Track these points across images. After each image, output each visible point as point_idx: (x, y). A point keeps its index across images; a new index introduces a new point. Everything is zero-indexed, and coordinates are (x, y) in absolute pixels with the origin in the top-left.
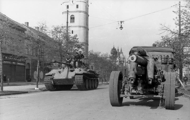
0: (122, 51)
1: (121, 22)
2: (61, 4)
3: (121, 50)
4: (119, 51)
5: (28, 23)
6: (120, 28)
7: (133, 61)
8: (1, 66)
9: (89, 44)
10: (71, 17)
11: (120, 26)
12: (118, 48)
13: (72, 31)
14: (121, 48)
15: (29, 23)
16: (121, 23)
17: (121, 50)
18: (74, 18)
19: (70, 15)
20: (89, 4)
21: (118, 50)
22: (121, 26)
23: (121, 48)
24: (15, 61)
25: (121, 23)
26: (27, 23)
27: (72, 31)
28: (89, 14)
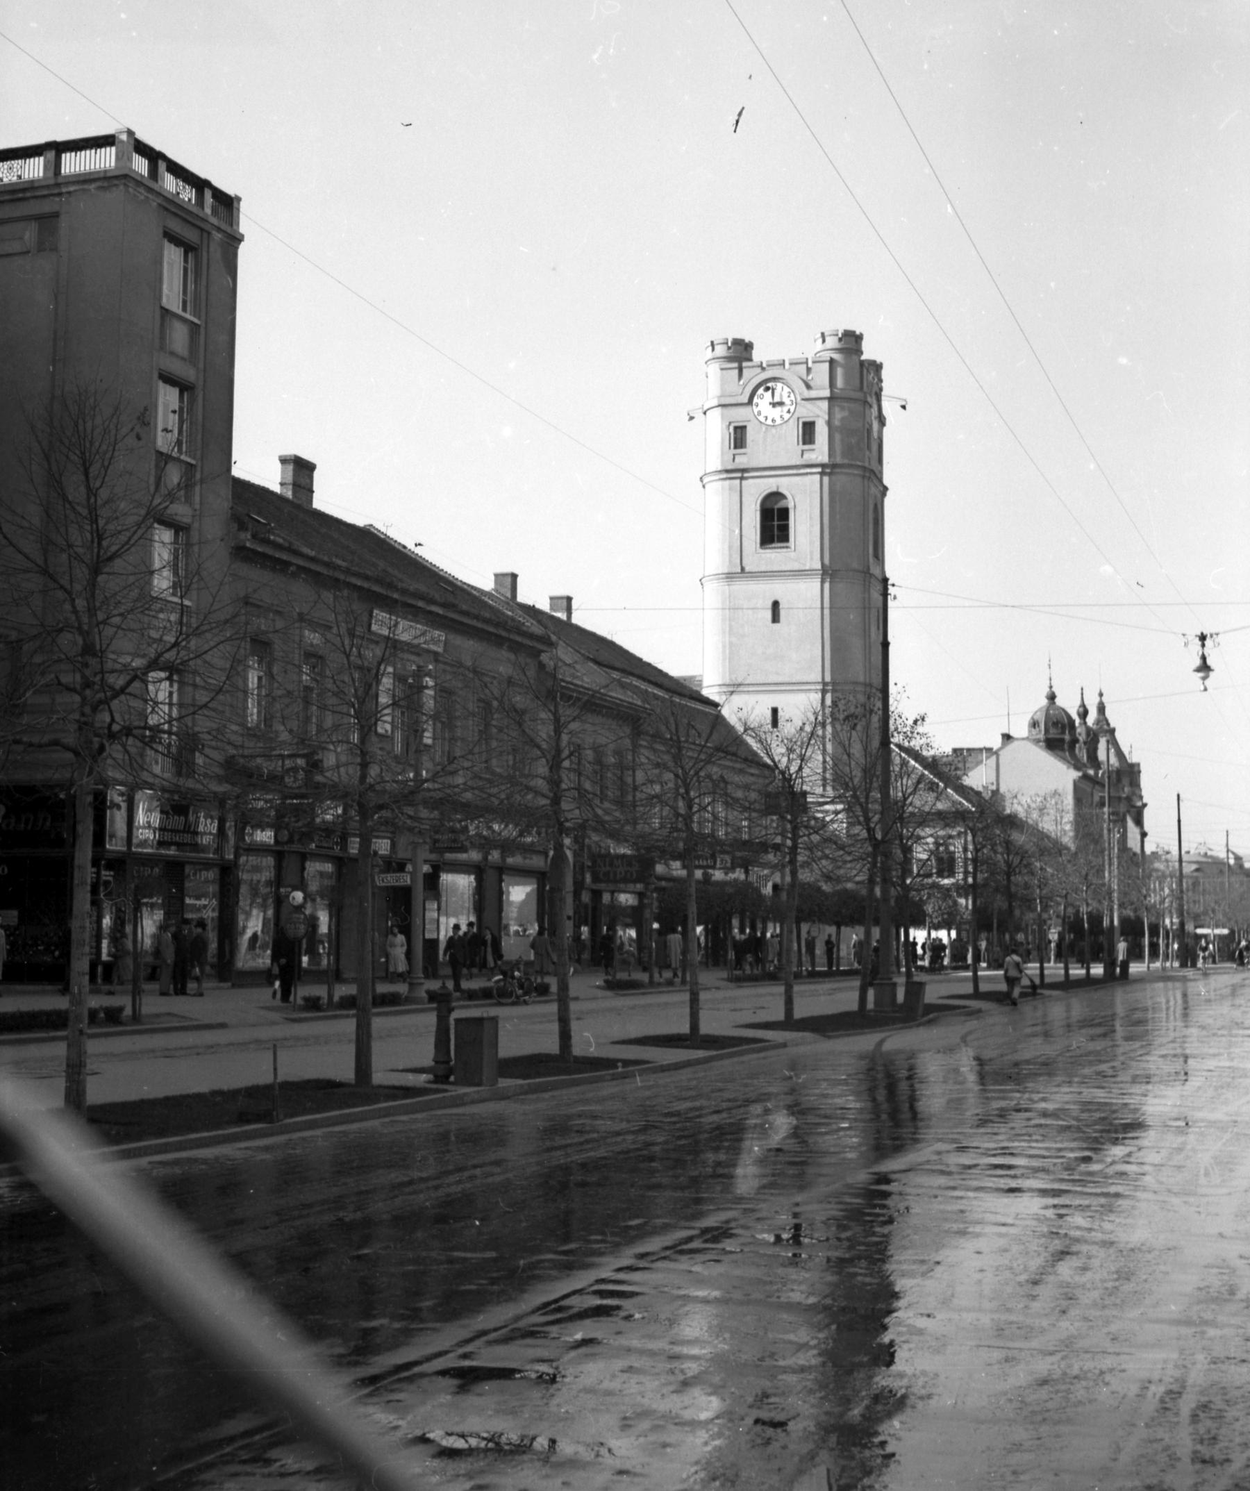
0: (1108, 713)
1: (1203, 638)
2: (692, 418)
3: (1101, 709)
4: (1057, 700)
5: (514, 577)
6: (1198, 670)
7: (612, 746)
8: (690, 896)
9: (315, 488)
10: (768, 505)
11: (1198, 662)
12: (1079, 703)
13: (776, 605)
14: (1101, 695)
15: (519, 580)
16: (1203, 646)
17: (1101, 709)
18: (784, 513)
19: (756, 489)
20: (885, 412)
21: (1084, 714)
22: (1204, 658)
23: (1101, 695)
24: (966, 866)
25: (1203, 646)
26: (509, 579)
27: (776, 605)
28: (886, 482)
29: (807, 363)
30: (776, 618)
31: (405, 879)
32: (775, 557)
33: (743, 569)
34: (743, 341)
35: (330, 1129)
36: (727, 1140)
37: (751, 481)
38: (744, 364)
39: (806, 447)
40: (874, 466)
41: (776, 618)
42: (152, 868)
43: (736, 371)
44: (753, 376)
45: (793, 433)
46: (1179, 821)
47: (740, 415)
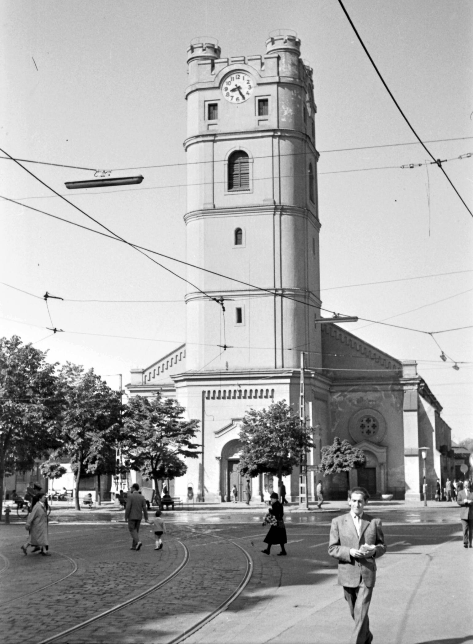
19: (225, 149)
29: (261, 59)
30: (238, 241)
31: (347, 469)
32: (238, 199)
33: (214, 207)
34: (313, 88)
35: (124, 604)
36: (131, 634)
37: (218, 143)
38: (216, 61)
39: (261, 117)
40: (309, 133)
41: (238, 241)
42: (153, 450)
43: (210, 66)
44: (221, 69)
45: (252, 107)
46: (55, 298)
47: (211, 96)
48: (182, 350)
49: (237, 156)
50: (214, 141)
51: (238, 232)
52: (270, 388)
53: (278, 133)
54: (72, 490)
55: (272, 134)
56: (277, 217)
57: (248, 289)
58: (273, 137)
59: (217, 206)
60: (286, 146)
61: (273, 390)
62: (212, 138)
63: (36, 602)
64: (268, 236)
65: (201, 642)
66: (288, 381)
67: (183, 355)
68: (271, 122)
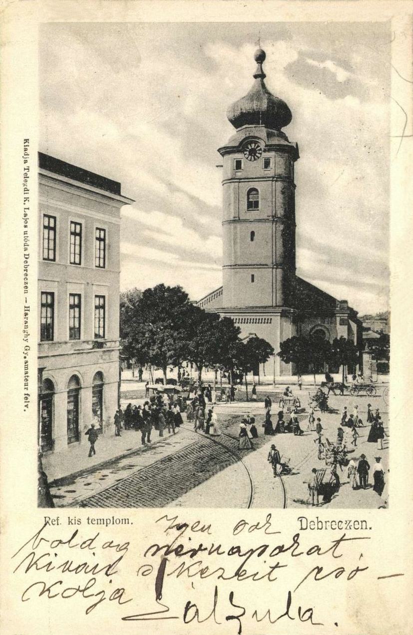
19: (245, 187)
32: (253, 215)
48: (220, 290)
49: (252, 191)
50: (239, 182)
51: (253, 234)
52: (270, 318)
53: (277, 178)
54: (104, 337)
55: (271, 179)
56: (274, 225)
57: (245, 559)
58: (273, 181)
59: (241, 219)
60: (279, 185)
61: (271, 319)
62: (238, 181)
63: (160, 452)
64: (268, 232)
65: (384, 434)
66: (279, 314)
67: (221, 293)
68: (270, 172)
